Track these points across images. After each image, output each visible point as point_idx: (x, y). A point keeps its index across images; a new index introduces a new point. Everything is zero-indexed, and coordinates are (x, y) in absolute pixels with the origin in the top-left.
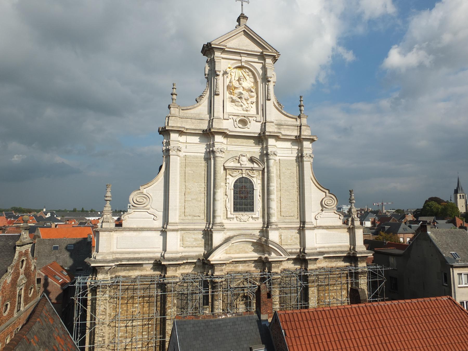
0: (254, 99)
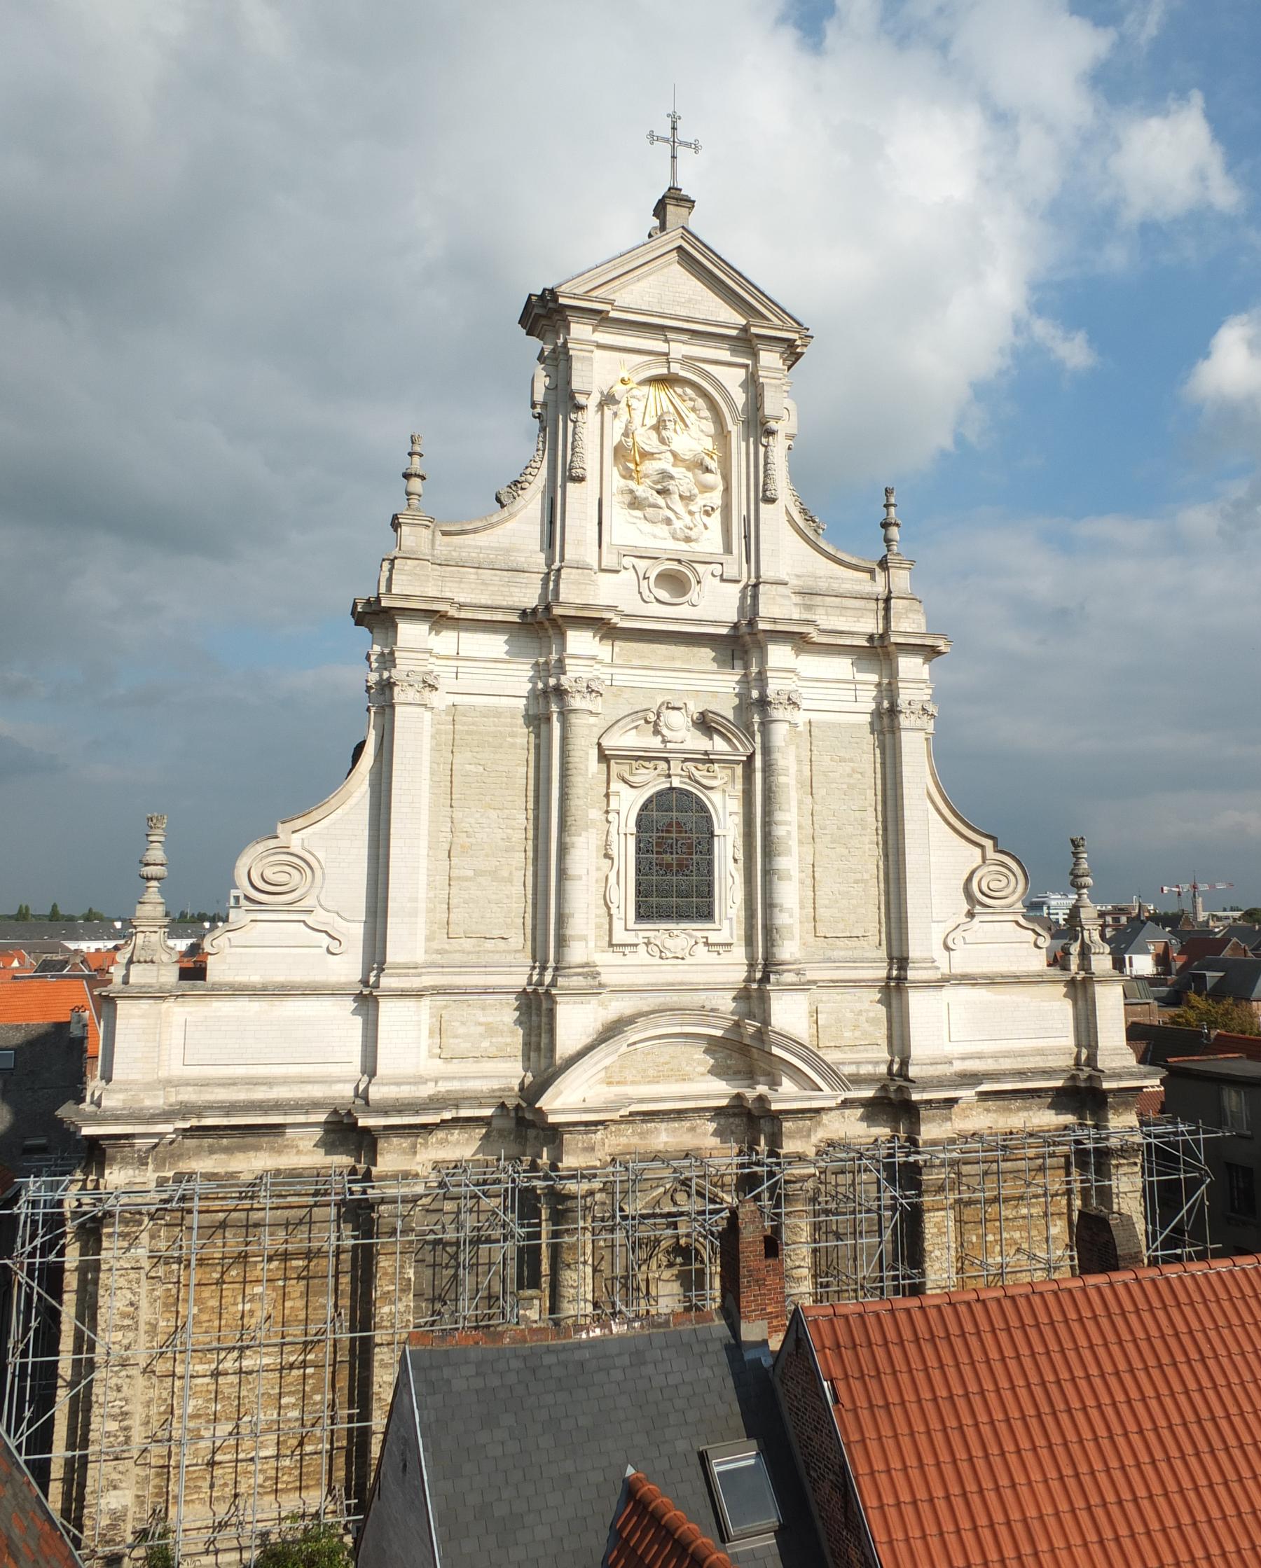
0: (715, 498)
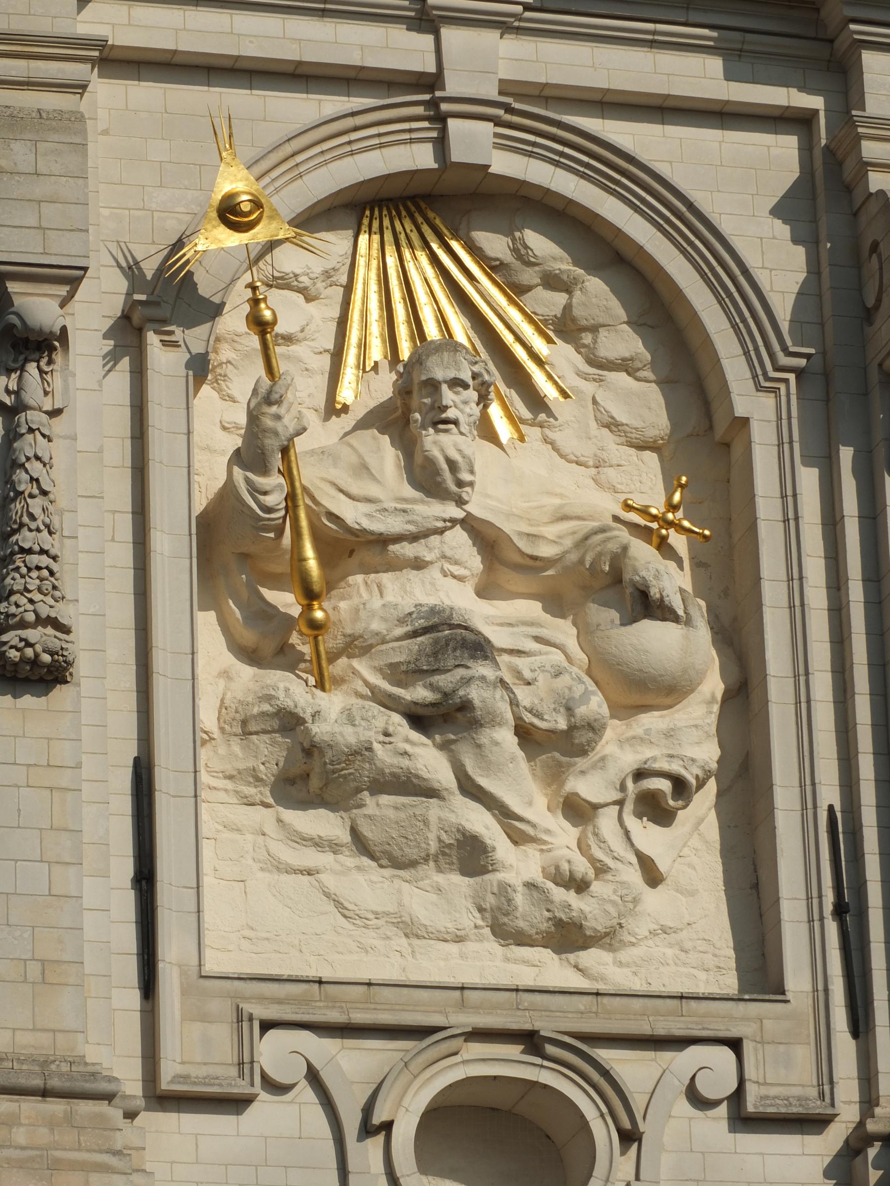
0: (691, 735)
